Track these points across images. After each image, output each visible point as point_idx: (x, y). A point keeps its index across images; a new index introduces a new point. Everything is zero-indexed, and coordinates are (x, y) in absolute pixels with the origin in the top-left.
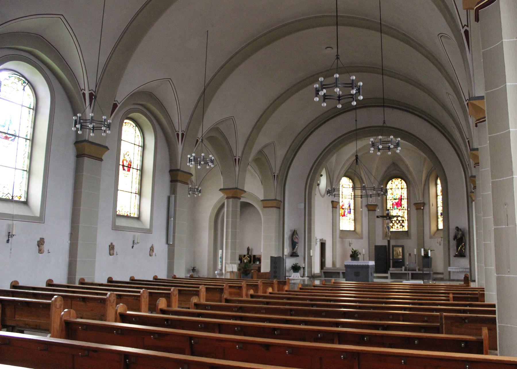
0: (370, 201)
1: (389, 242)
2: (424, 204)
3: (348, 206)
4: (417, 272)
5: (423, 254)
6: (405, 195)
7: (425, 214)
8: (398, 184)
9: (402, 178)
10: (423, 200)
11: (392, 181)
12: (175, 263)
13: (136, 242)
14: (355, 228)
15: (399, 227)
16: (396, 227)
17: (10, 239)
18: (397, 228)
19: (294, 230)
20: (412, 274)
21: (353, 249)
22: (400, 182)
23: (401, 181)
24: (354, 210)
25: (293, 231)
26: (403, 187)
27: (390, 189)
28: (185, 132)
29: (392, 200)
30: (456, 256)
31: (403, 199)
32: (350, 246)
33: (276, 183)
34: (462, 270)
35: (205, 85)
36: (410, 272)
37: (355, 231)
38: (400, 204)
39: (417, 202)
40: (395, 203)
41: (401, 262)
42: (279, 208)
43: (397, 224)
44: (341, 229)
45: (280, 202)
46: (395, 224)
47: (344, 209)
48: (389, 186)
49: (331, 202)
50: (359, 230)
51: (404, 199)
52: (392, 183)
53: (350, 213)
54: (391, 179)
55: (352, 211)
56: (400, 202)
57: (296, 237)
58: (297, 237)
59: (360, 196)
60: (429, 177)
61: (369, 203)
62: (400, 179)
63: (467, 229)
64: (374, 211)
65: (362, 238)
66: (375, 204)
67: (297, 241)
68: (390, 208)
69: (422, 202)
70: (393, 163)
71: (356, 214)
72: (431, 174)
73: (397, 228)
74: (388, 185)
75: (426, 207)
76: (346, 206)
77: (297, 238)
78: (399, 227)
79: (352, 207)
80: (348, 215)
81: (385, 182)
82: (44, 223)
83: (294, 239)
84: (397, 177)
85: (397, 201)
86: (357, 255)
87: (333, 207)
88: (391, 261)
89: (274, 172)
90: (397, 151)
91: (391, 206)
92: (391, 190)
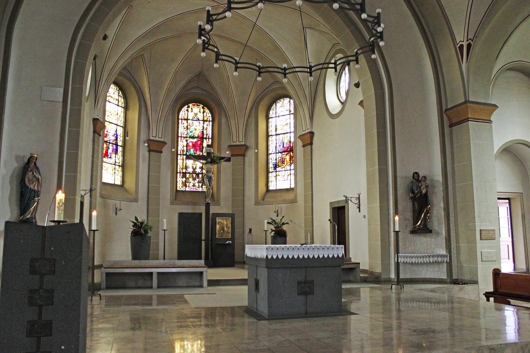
1: (208, 206)
2: (246, 148)
3: (114, 138)
6: (209, 132)
7: (247, 164)
8: (199, 113)
9: (206, 105)
10: (245, 141)
11: (189, 107)
12: (478, 267)
13: (118, 208)
14: (123, 181)
15: (197, 185)
16: (191, 185)
18: (194, 185)
19: (29, 156)
21: (136, 219)
22: (202, 110)
23: (203, 108)
24: (124, 147)
25: (26, 161)
26: (205, 119)
27: (184, 119)
29: (186, 139)
30: (414, 232)
31: (206, 138)
32: (116, 214)
34: (436, 259)
38: (198, 145)
39: (233, 144)
40: (191, 144)
41: (229, 244)
43: (194, 179)
46: (191, 180)
48: (183, 114)
50: (130, 184)
51: (207, 139)
52: (188, 110)
53: (116, 153)
54: (186, 103)
55: (120, 149)
56: (199, 143)
57: (35, 177)
58: (37, 175)
60: (259, 104)
61: (152, 138)
62: (201, 106)
63: (439, 177)
64: (158, 154)
65: (136, 200)
66: (162, 140)
67: (36, 188)
68: (183, 151)
69: (243, 143)
71: (126, 154)
72: (261, 99)
73: (194, 185)
74: (181, 113)
75: (250, 154)
76: (111, 138)
77: (38, 180)
78: (197, 185)
79: (120, 143)
80: (113, 155)
83: (27, 182)
84: (197, 101)
85: (195, 140)
86: (146, 232)
87: (95, 132)
88: (203, 243)
90: (301, 3)
91: (185, 148)
92: (185, 121)
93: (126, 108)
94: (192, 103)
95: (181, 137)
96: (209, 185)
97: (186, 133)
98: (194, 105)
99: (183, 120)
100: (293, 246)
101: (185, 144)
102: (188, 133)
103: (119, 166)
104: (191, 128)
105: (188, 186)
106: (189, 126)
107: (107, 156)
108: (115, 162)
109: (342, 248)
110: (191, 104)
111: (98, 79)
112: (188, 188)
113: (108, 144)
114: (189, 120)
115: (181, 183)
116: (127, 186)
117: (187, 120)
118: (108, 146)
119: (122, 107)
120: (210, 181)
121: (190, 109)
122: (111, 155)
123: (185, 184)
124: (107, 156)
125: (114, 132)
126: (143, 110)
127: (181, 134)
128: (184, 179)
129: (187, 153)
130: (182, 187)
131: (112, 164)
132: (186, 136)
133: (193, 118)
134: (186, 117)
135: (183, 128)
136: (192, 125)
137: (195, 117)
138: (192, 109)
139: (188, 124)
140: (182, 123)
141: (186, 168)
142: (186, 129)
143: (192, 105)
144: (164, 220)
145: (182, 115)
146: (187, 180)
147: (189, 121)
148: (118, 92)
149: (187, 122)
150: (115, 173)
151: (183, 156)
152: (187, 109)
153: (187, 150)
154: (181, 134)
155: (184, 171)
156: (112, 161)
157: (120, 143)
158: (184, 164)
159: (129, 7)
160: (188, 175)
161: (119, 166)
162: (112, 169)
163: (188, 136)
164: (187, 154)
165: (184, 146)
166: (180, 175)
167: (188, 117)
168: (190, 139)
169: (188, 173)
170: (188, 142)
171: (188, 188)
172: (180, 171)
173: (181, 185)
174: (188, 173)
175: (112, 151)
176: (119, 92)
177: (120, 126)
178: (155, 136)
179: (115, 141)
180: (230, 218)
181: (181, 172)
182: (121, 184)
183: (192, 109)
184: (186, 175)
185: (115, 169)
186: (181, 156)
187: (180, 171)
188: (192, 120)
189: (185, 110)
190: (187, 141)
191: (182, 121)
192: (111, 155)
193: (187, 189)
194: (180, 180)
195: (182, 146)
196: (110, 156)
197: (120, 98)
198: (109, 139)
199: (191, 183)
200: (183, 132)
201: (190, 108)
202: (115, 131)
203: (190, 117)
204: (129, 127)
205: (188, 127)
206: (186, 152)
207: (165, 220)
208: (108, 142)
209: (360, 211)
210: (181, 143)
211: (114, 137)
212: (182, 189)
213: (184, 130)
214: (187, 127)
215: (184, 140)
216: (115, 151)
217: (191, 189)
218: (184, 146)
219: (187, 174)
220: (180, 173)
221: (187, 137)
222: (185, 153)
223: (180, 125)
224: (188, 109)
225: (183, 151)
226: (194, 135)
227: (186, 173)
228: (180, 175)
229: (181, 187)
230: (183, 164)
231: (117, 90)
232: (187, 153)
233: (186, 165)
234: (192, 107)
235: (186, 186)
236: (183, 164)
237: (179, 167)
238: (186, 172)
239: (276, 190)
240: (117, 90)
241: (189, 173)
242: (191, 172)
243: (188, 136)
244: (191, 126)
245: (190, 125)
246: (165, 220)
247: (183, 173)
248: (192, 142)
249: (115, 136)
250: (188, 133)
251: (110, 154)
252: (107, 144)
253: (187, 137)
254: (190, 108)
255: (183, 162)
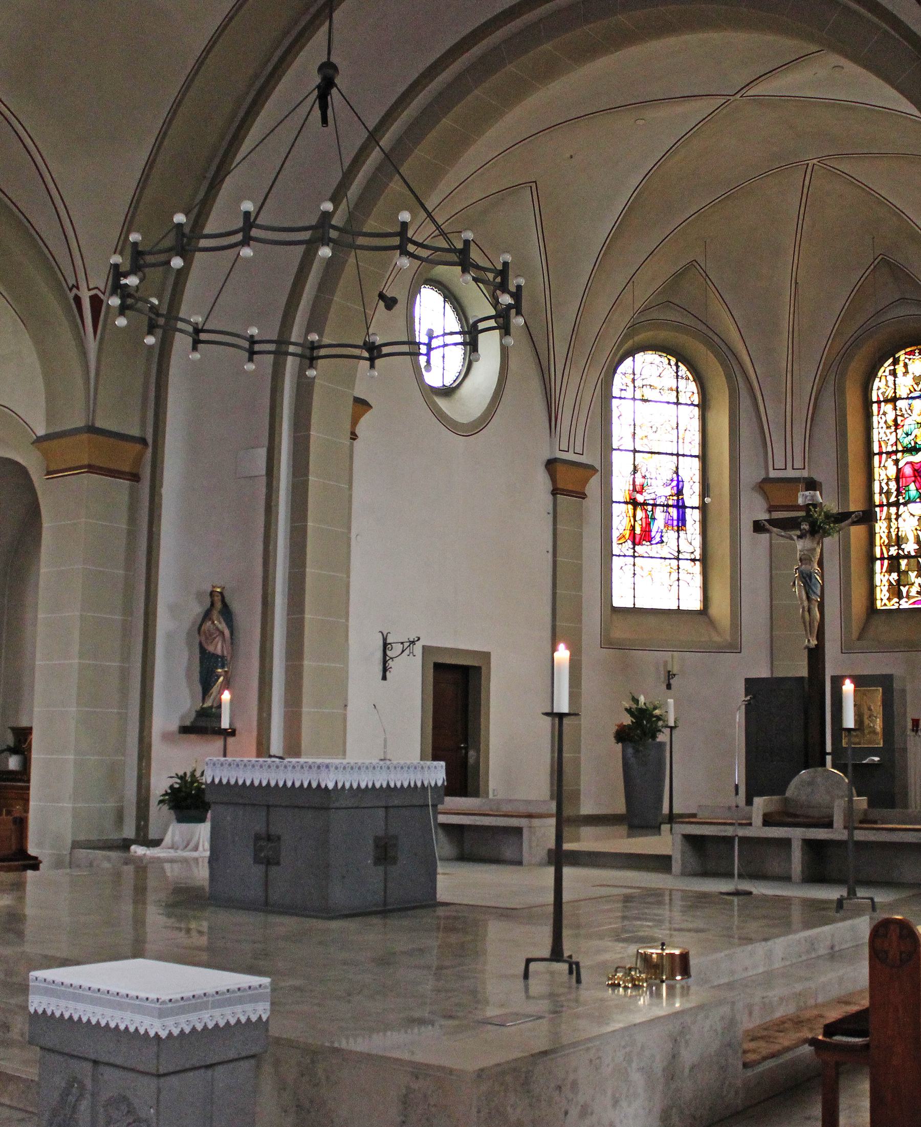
0: (779, 464)
4: (838, 833)
5: (144, 761)
11: (896, 362)
17: (672, 681)
20: (809, 844)
24: (703, 508)
27: (887, 401)
28: (104, 293)
29: (894, 457)
32: (669, 686)
33: (92, 345)
35: (327, 23)
36: (797, 834)
37: (704, 611)
40: (908, 471)
41: (873, 765)
42: (135, 477)
44: (615, 605)
45: (138, 447)
47: (645, 504)
48: (881, 387)
49: (543, 468)
50: (721, 608)
52: (894, 373)
53: (681, 522)
55: (693, 517)
59: (246, 344)
61: (773, 474)
65: (734, 647)
70: (886, 262)
71: (710, 533)
79: (692, 497)
80: (670, 536)
81: (856, 367)
82: (842, 653)
89: (71, 282)
91: (893, 485)
92: (888, 408)
93: (704, 406)
94: (904, 349)
95: (880, 454)
96: (804, 597)
97: (893, 439)
98: (912, 353)
99: (883, 404)
100: (238, 759)
101: (892, 471)
102: (897, 439)
103: (693, 560)
104: (907, 422)
105: (905, 595)
106: (899, 419)
107: (650, 541)
108: (679, 552)
109: (442, 766)
110: (903, 352)
111: (545, 363)
112: (905, 600)
113: (650, 508)
114: (901, 399)
115: (887, 587)
116: (714, 611)
117: (894, 400)
118: (650, 514)
119: (692, 404)
120: (810, 587)
121: (900, 369)
122: (662, 536)
123: (896, 591)
124: (650, 541)
125: (669, 475)
126: (745, 402)
127: (880, 446)
128: (894, 576)
129: (900, 498)
130: (889, 599)
131: (665, 558)
132: (894, 448)
133: (911, 392)
134: (890, 394)
135: (885, 426)
136: (909, 412)
137: (915, 386)
138: (906, 365)
139: (898, 413)
140: (881, 412)
141: (899, 541)
142: (893, 428)
143: (906, 354)
144: (669, 700)
145: (878, 389)
146: (902, 577)
147: (899, 404)
148: (674, 368)
149: (895, 409)
150: (678, 580)
151: (888, 509)
152: (892, 368)
153: (898, 490)
154: (880, 446)
155: (893, 551)
156: (668, 549)
157: (692, 497)
158: (892, 530)
159: (531, 187)
160: (903, 563)
161: (693, 560)
162: (669, 570)
163: (900, 448)
164: (898, 500)
165: (889, 479)
166: (882, 565)
167: (895, 392)
168: (905, 455)
169: (905, 557)
170: (901, 465)
171: (905, 600)
172: (882, 553)
173: (887, 595)
174: (905, 557)
175: (666, 525)
176: (677, 367)
177: (691, 456)
178: (795, 468)
179: (675, 498)
180: (880, 689)
181: (886, 556)
182: (702, 608)
183: (906, 365)
184: (899, 564)
185: (679, 568)
186: (881, 511)
187: (882, 553)
188: (908, 398)
189: (887, 373)
190: (896, 462)
191: (879, 407)
192: (662, 536)
193: (905, 604)
194: (882, 579)
195: (885, 481)
196: (658, 539)
197: (682, 383)
198: (653, 496)
199: (913, 584)
200: (885, 438)
201: (901, 364)
202: (671, 472)
203: (902, 392)
204: (712, 453)
205: (899, 422)
206: (897, 496)
207: (672, 700)
208: (649, 504)
209: (384, 678)
210: (883, 473)
211: (669, 488)
212: (890, 606)
213: (888, 431)
214: (895, 420)
215: (890, 464)
216: (675, 523)
217: (914, 603)
218: (889, 479)
219: (901, 561)
220: (882, 559)
221: (896, 452)
222: (893, 499)
223: (875, 419)
224: (895, 370)
225: (888, 494)
226: (916, 443)
227: (898, 557)
228: (882, 565)
229: (885, 601)
230: (889, 532)
231: (669, 364)
232: (900, 498)
233: (897, 534)
234: (907, 361)
235: (900, 596)
236: (889, 532)
237: (878, 542)
238: (898, 553)
239: (678, 611)
240: (669, 364)
241: (908, 556)
242: (913, 553)
243: (900, 448)
244: (906, 416)
245: (902, 416)
246: (672, 700)
247: (890, 558)
248: (911, 463)
249: (675, 483)
250: (897, 439)
251: (659, 535)
252: (646, 510)
253: (896, 452)
254: (901, 364)
255: (889, 527)
